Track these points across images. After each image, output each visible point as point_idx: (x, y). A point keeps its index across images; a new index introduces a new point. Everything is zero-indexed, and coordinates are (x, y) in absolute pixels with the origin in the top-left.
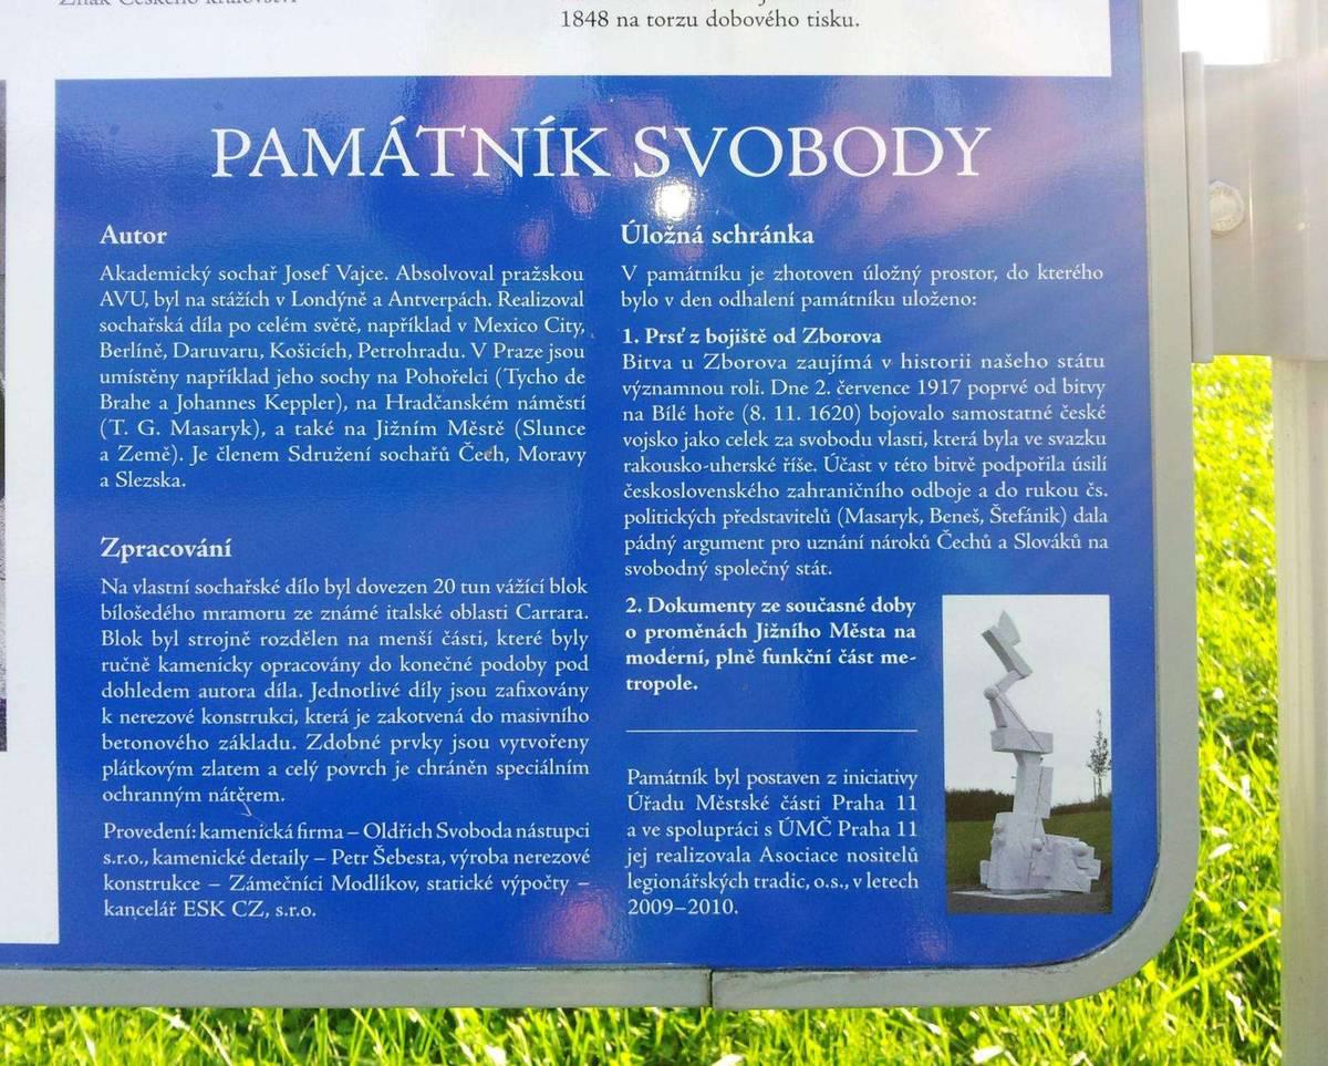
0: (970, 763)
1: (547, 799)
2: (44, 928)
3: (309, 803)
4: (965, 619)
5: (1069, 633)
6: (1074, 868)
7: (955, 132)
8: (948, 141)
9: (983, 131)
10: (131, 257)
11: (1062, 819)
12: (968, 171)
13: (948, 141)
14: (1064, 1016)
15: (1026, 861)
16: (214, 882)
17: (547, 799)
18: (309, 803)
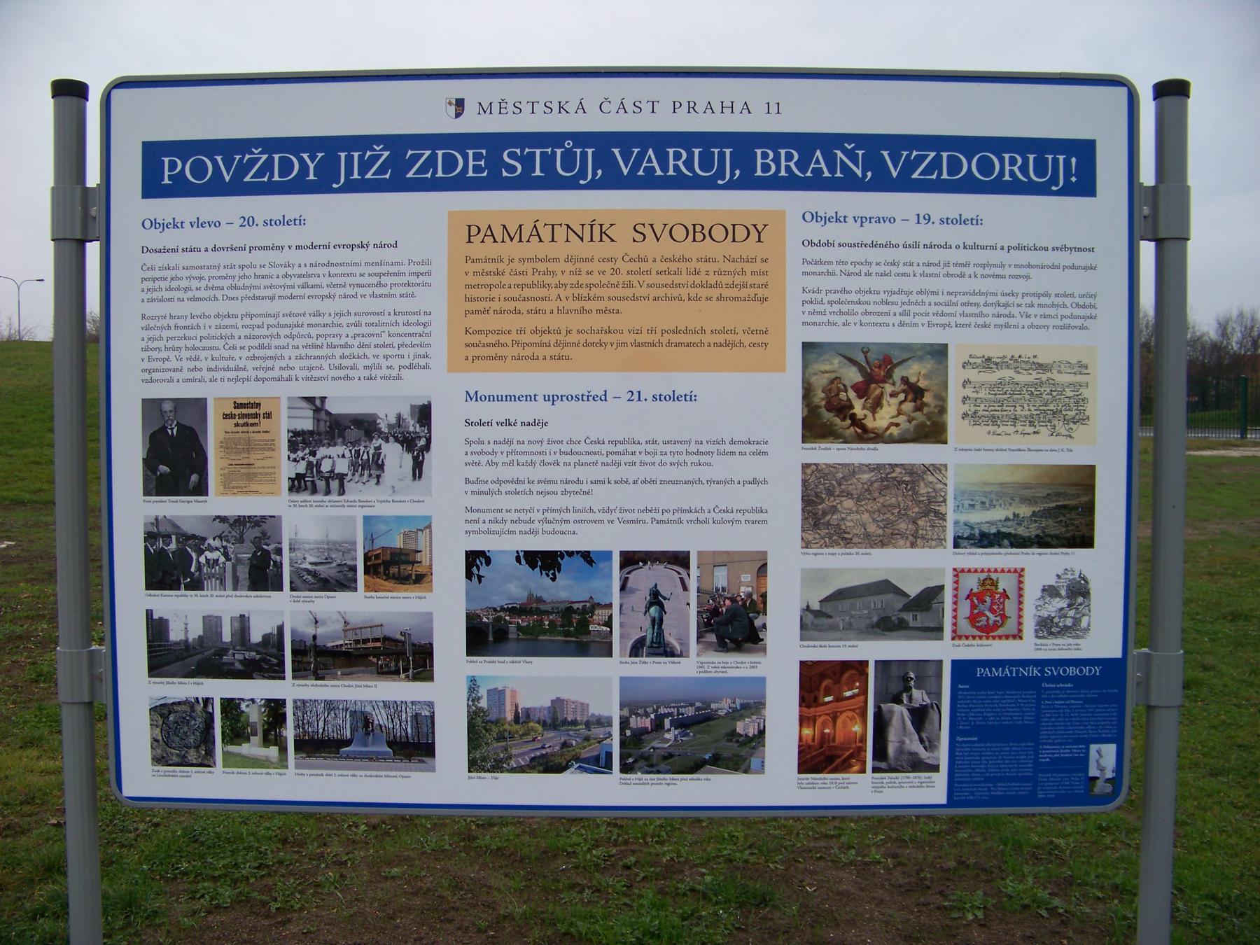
0: (1093, 772)
1: (1026, 779)
2: (944, 801)
3: (988, 780)
4: (1094, 748)
5: (1110, 750)
6: (1109, 788)
7: (305, 156)
8: (301, 160)
9: (320, 155)
10: (963, 690)
11: (1108, 780)
12: (311, 177)
13: (301, 160)
14: (745, 707)
15: (1101, 788)
16: (972, 793)
17: (1026, 779)
18: (988, 780)
